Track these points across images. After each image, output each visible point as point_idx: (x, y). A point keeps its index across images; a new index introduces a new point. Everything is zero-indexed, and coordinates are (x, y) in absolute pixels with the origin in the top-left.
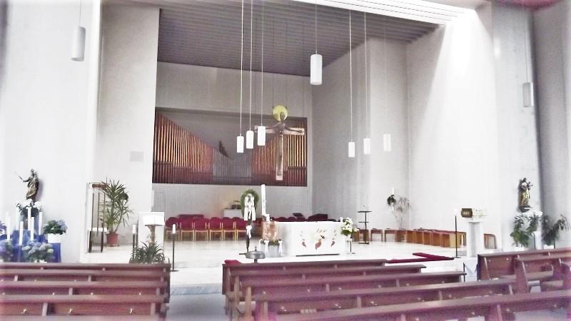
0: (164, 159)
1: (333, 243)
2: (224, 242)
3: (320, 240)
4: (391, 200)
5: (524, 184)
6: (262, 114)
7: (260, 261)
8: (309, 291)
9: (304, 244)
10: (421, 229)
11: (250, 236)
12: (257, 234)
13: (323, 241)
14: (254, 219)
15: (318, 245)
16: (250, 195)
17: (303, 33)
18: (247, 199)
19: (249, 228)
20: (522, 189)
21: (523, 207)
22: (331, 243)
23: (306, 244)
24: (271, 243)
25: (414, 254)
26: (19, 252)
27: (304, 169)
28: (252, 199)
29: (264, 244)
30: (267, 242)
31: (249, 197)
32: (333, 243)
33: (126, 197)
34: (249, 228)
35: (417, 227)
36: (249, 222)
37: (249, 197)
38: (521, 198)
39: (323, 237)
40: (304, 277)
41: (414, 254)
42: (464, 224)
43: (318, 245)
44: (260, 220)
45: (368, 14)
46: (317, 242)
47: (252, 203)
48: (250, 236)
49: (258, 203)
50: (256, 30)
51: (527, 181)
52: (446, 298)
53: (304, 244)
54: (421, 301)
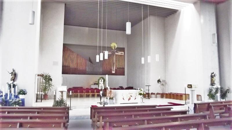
0: (67, 64)
1: (135, 98)
2: (91, 98)
3: (130, 97)
4: (159, 81)
5: (213, 75)
6: (106, 46)
7: (106, 106)
8: (125, 118)
9: (123, 99)
10: (171, 93)
11: (102, 96)
12: (104, 95)
13: (131, 97)
14: (103, 89)
15: (129, 99)
16: (102, 79)
17: (123, 13)
18: (100, 80)
19: (101, 92)
20: (212, 77)
21: (212, 84)
22: (135, 98)
23: (124, 99)
24: (110, 98)
25: (168, 103)
26: (8, 102)
27: (124, 69)
28: (103, 80)
29: (107, 99)
30: (108, 98)
31: (101, 80)
32: (135, 98)
33: (51, 80)
34: (101, 92)
35: (170, 92)
36: (101, 90)
37: (101, 80)
38: (212, 80)
39: (131, 96)
40: (123, 112)
41: (168, 103)
42: (188, 91)
43: (129, 99)
44: (106, 89)
45: (149, 6)
46: (129, 98)
47: (103, 82)
48: (102, 96)
49: (105, 82)
50: (104, 12)
51: (214, 73)
52: (181, 121)
53: (123, 99)
54: (171, 122)
